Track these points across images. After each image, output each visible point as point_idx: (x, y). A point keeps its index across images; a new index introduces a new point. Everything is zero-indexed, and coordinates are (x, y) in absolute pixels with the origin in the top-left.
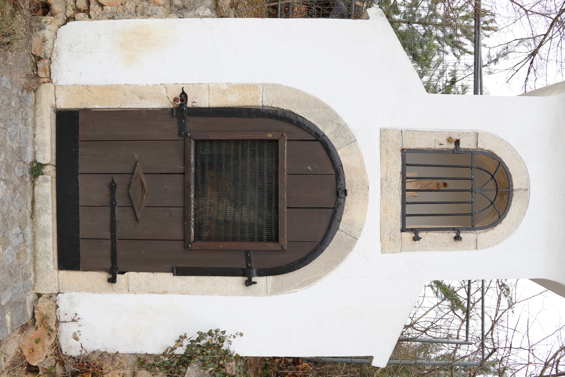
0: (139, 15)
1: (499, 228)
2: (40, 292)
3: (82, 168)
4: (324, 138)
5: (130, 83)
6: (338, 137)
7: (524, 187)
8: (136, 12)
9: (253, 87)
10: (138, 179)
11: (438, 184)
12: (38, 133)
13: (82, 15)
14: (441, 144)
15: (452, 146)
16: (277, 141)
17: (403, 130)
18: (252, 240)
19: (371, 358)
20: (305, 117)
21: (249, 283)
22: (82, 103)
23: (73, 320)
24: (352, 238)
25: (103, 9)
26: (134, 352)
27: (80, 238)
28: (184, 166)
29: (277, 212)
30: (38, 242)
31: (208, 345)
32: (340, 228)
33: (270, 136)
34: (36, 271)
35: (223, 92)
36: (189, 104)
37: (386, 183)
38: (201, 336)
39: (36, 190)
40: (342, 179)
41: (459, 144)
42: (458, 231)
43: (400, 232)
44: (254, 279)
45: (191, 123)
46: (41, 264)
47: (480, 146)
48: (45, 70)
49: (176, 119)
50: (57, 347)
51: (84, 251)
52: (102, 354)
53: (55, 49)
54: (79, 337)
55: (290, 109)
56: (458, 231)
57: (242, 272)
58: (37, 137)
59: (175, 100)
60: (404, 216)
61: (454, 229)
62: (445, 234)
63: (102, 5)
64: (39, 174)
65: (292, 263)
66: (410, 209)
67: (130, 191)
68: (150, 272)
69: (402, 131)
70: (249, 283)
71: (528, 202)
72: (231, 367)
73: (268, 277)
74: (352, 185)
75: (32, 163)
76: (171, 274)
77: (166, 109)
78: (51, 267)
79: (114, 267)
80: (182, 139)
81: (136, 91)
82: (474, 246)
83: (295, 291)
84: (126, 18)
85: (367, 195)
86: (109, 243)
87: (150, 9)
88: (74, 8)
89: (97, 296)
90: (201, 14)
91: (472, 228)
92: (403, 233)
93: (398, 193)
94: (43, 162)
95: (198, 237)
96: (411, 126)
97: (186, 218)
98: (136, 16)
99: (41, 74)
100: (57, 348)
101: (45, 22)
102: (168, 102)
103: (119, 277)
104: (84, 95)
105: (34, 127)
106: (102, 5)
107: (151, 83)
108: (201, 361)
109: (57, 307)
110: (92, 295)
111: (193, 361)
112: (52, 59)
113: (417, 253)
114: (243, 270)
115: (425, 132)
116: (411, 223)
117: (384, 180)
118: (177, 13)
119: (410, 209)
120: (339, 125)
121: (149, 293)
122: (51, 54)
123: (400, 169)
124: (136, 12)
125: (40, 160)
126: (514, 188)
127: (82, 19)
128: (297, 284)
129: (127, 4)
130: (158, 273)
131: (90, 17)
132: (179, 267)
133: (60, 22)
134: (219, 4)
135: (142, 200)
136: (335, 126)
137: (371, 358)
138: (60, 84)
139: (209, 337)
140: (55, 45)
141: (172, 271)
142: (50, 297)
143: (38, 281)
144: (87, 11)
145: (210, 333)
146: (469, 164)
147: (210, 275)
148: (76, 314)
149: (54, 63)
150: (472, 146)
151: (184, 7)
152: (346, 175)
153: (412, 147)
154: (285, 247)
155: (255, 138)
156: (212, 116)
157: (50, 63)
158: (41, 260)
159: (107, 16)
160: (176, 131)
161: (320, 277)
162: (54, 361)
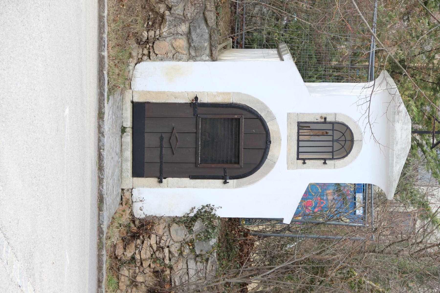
1: (346, 158)
2: (123, 188)
7: (360, 139)
8: (173, 58)
9: (229, 94)
10: (175, 135)
14: (317, 119)
15: (323, 120)
16: (239, 119)
20: (252, 108)
21: (225, 183)
22: (146, 99)
24: (273, 163)
27: (145, 162)
30: (123, 164)
31: (206, 212)
33: (236, 116)
34: (122, 178)
35: (215, 96)
36: (199, 101)
38: (203, 207)
39: (123, 139)
43: (296, 160)
44: (228, 181)
45: (199, 110)
46: (124, 175)
49: (192, 108)
50: (132, 214)
51: (147, 168)
53: (134, 75)
54: (143, 209)
55: (245, 104)
57: (222, 178)
58: (123, 114)
60: (298, 153)
65: (245, 174)
68: (178, 177)
69: (298, 114)
70: (225, 183)
71: (362, 146)
72: (216, 223)
73: (234, 180)
74: (274, 139)
76: (189, 179)
78: (129, 176)
79: (161, 175)
80: (196, 117)
81: (173, 94)
83: (246, 186)
85: (280, 143)
86: (159, 164)
89: (152, 189)
91: (333, 159)
93: (296, 142)
98: (173, 60)
103: (163, 180)
107: (180, 91)
108: (202, 219)
110: (150, 189)
111: (198, 219)
112: (132, 79)
113: (304, 170)
114: (223, 176)
116: (300, 157)
117: (289, 137)
123: (297, 131)
124: (173, 58)
126: (354, 140)
128: (247, 183)
130: (182, 178)
132: (192, 175)
135: (176, 145)
137: (283, 219)
139: (206, 208)
140: (134, 73)
141: (190, 177)
143: (122, 183)
145: (207, 206)
147: (207, 179)
152: (271, 134)
154: (242, 167)
156: (209, 107)
158: (125, 173)
159: (159, 59)
160: (192, 113)
161: (258, 180)
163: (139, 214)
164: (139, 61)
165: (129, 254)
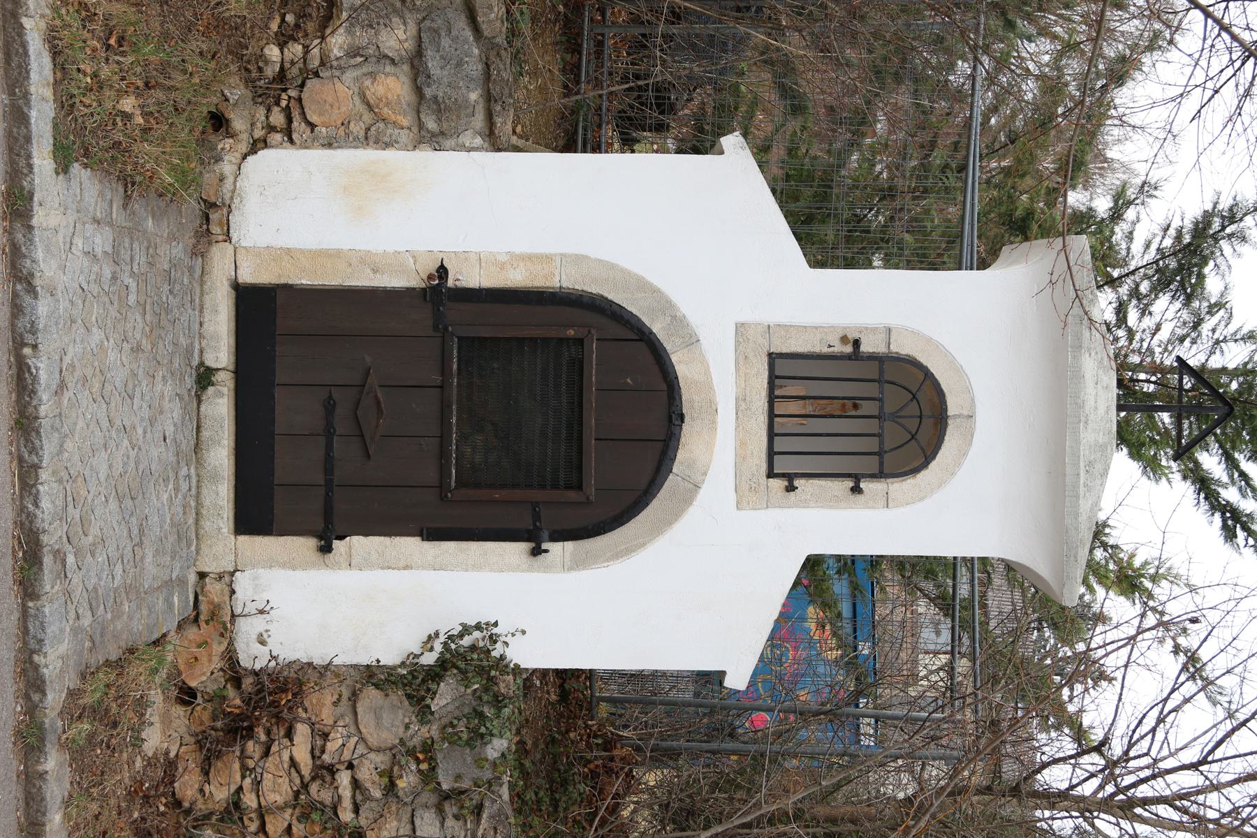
0: (371, 144)
1: (923, 476)
3: (280, 377)
4: (652, 337)
5: (357, 248)
6: (672, 335)
7: (965, 413)
8: (366, 138)
9: (547, 258)
11: (844, 406)
12: (206, 320)
13: (278, 137)
17: (771, 324)
18: (543, 487)
22: (280, 275)
23: (262, 612)
25: (312, 131)
26: (354, 662)
28: (442, 376)
29: (581, 375)
30: (204, 491)
32: (674, 470)
33: (571, 332)
35: (502, 266)
36: (450, 283)
37: (743, 404)
38: (466, 630)
39: (203, 408)
40: (677, 398)
42: (857, 478)
43: (765, 478)
44: (545, 546)
46: (207, 525)
47: (894, 348)
48: (220, 224)
52: (303, 667)
53: (237, 191)
54: (268, 640)
56: (857, 478)
58: (205, 326)
59: (430, 277)
60: (771, 454)
61: (849, 476)
62: (836, 483)
63: (312, 126)
64: (209, 384)
66: (780, 444)
67: (358, 413)
70: (537, 552)
71: (972, 436)
72: (508, 685)
75: (198, 367)
77: (414, 289)
78: (225, 530)
81: (367, 260)
82: (883, 502)
84: (350, 147)
85: (714, 422)
86: (322, 491)
88: (265, 125)
89: (299, 574)
90: (467, 145)
91: (880, 475)
93: (763, 419)
94: (213, 365)
95: (460, 483)
97: (443, 454)
99: (215, 229)
100: (231, 658)
101: (222, 149)
102: (418, 278)
103: (336, 543)
105: (201, 311)
106: (312, 126)
107: (390, 249)
110: (290, 572)
111: (449, 673)
112: (233, 206)
113: (791, 510)
114: (528, 531)
116: (781, 465)
117: (741, 400)
118: (430, 142)
119: (780, 444)
120: (674, 317)
121: (383, 568)
122: (232, 198)
124: (366, 138)
125: (210, 362)
127: (279, 145)
128: (609, 554)
129: (352, 125)
131: (291, 141)
133: (243, 147)
134: (496, 132)
135: (377, 426)
137: (722, 674)
138: (243, 245)
140: (238, 184)
142: (220, 578)
143: (201, 552)
144: (288, 133)
146: (876, 377)
147: (478, 540)
148: (268, 602)
149: (235, 212)
150: (881, 349)
151: (442, 133)
154: (592, 498)
155: (548, 335)
157: (229, 212)
159: (321, 141)
161: (643, 545)
162: (223, 680)
163: (252, 655)
164: (257, 145)
165: (220, 794)
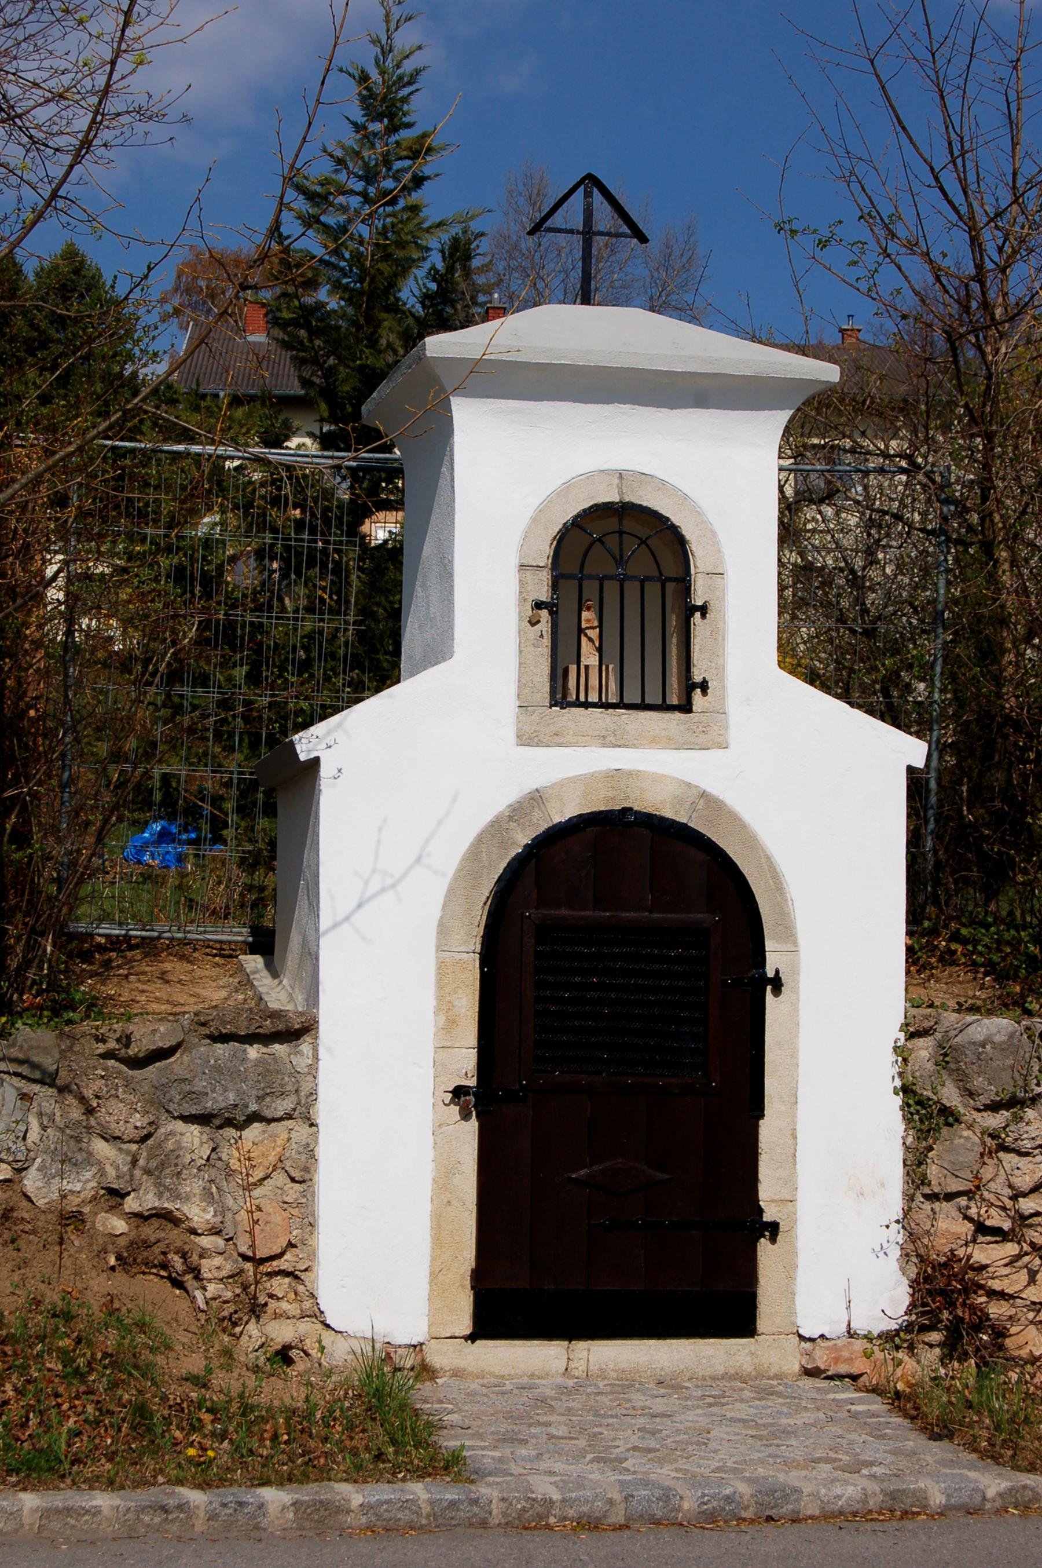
7: (616, 481)
9: (442, 969)
14: (542, 636)
19: (911, 770)
21: (777, 984)
37: (608, 739)
41: (543, 603)
60: (665, 707)
76: (761, 1122)
83: (790, 903)
85: (630, 773)
87: (298, 1156)
92: (694, 708)
96: (512, 689)
103: (767, 1218)
104: (447, 1281)
109: (822, 1336)
115: (520, 664)
120: (511, 818)
121: (795, 1164)
128: (779, 899)
136: (512, 825)
137: (911, 770)
150: (545, 576)
153: (547, 688)
161: (768, 858)
